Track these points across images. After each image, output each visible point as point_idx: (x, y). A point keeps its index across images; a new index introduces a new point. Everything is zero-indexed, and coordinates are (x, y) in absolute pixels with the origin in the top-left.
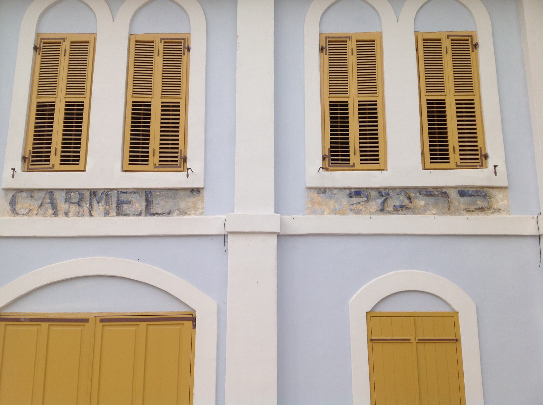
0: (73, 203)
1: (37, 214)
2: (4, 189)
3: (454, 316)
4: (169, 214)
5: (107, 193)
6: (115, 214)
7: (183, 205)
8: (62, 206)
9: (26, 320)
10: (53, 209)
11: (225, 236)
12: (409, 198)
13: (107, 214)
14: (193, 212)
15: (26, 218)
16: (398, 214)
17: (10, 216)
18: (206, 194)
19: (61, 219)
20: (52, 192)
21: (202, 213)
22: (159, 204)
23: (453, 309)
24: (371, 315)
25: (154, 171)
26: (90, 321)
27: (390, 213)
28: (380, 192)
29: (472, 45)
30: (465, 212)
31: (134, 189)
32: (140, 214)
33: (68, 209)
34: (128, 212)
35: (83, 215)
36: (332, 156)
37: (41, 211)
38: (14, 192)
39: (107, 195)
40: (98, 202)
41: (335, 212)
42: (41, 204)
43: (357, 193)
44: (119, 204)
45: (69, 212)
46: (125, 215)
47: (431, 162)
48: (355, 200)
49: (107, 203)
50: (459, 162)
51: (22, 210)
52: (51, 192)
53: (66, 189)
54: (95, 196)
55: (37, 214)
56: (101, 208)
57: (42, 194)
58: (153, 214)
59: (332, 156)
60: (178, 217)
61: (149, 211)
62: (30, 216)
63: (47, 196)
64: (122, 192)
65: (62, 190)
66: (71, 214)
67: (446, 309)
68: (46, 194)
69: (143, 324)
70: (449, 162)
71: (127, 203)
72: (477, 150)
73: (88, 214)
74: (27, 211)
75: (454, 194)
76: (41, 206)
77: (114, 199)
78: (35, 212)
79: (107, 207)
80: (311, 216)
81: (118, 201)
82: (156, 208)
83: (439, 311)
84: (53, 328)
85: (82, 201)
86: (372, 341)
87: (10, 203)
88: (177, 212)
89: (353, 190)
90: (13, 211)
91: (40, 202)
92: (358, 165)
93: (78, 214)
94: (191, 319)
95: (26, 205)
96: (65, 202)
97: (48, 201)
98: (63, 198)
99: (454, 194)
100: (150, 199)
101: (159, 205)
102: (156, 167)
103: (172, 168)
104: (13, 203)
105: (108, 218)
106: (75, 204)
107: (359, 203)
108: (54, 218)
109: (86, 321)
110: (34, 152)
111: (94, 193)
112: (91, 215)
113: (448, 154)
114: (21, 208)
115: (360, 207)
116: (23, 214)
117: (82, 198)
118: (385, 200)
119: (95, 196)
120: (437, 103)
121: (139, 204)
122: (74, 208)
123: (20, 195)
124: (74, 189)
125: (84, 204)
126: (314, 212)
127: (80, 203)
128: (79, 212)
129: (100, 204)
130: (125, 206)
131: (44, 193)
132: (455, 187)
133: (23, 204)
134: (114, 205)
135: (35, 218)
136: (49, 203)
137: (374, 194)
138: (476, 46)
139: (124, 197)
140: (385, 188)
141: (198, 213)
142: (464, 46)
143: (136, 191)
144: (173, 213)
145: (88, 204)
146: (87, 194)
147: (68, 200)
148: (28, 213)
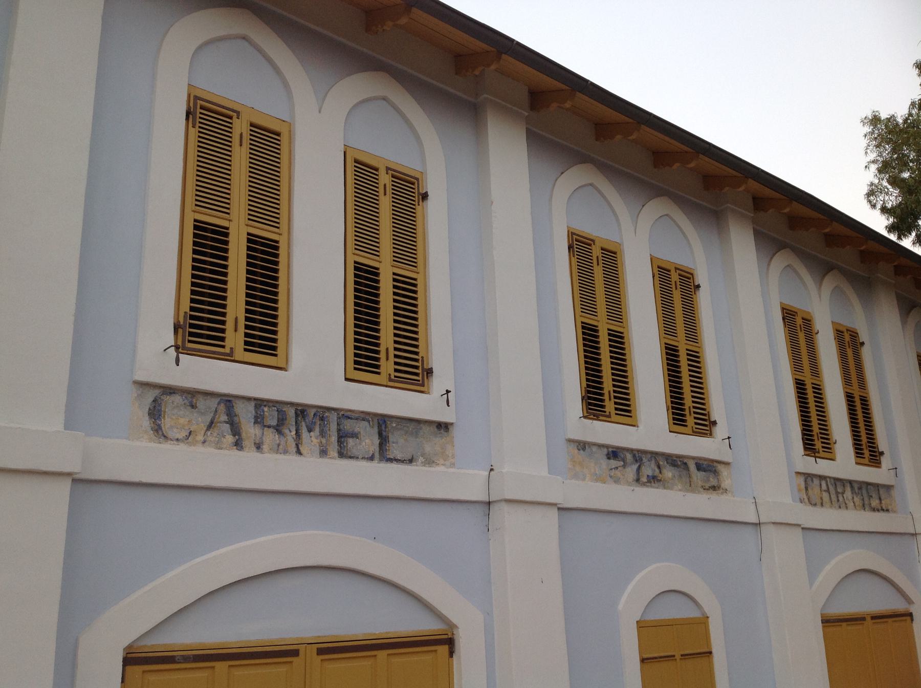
0: (269, 427)
1: (204, 442)
2: (570, 441)
3: (704, 621)
4: (411, 461)
5: (322, 413)
6: (336, 455)
7: (428, 448)
8: (250, 430)
9: (186, 659)
10: (234, 435)
11: (489, 503)
12: (659, 467)
13: (323, 453)
14: (441, 461)
15: (182, 447)
16: (652, 487)
17: (150, 440)
18: (456, 432)
19: (249, 455)
20: (230, 401)
21: (453, 465)
22: (397, 443)
23: (704, 613)
24: (641, 625)
25: (386, 386)
26: (301, 653)
27: (644, 484)
28: (634, 456)
29: (419, 193)
30: (702, 490)
31: (363, 412)
32: (371, 458)
33: (261, 438)
34: (355, 452)
35: (286, 452)
36: (192, 326)
37: (212, 436)
38: (157, 392)
39: (322, 419)
40: (310, 430)
41: (598, 479)
42: (212, 423)
43: (614, 453)
44: (342, 437)
45: (262, 443)
46: (351, 457)
47: (245, 350)
48: (614, 463)
49: (323, 434)
50: (393, 374)
51: (175, 430)
52: (228, 401)
53: (255, 399)
54: (304, 417)
55: (204, 442)
56: (315, 441)
57: (213, 403)
58: (390, 460)
59: (192, 326)
60: (424, 468)
61: (383, 454)
62: (190, 444)
63: (222, 407)
64: (345, 415)
65: (249, 399)
66: (265, 447)
67: (694, 613)
68: (219, 404)
69: (382, 654)
70: (276, 355)
71: (352, 437)
72: (416, 360)
73: (295, 450)
74: (184, 434)
75: (692, 466)
76: (211, 425)
77: (334, 427)
78: (200, 438)
79: (324, 441)
80: (573, 481)
81: (339, 430)
82: (395, 450)
83: (691, 616)
84: (238, 672)
85: (283, 424)
86: (643, 661)
87: (149, 414)
88: (421, 459)
89: (610, 450)
90: (157, 431)
91: (208, 419)
92: (240, 353)
93: (278, 449)
94: (447, 641)
95: (182, 421)
96: (255, 423)
97: (224, 418)
98: (250, 415)
99: (692, 466)
100: (384, 433)
101: (399, 444)
102: (390, 380)
103: (402, 382)
104: (155, 413)
105: (325, 461)
106: (271, 430)
107: (617, 468)
108: (235, 452)
109: (295, 653)
110: (192, 317)
111: (303, 412)
112: (299, 452)
113: (223, 331)
114: (172, 427)
115: (618, 473)
116: (177, 440)
117: (283, 420)
118: (639, 467)
119: (304, 417)
120: (213, 232)
121: (369, 441)
122: (270, 437)
123: (168, 399)
124: (268, 401)
125: (287, 431)
126: (575, 476)
127: (280, 428)
128: (279, 445)
129: (312, 433)
130: (351, 442)
131: (217, 400)
132: (694, 458)
133: (176, 417)
134: (334, 438)
135: (200, 449)
136: (227, 423)
137: (629, 456)
138: (425, 196)
139: (348, 425)
140: (638, 451)
141: (448, 463)
142: (409, 191)
143: (365, 416)
144: (417, 460)
145: (294, 433)
146: (291, 412)
147: (259, 420)
148: (187, 437)
